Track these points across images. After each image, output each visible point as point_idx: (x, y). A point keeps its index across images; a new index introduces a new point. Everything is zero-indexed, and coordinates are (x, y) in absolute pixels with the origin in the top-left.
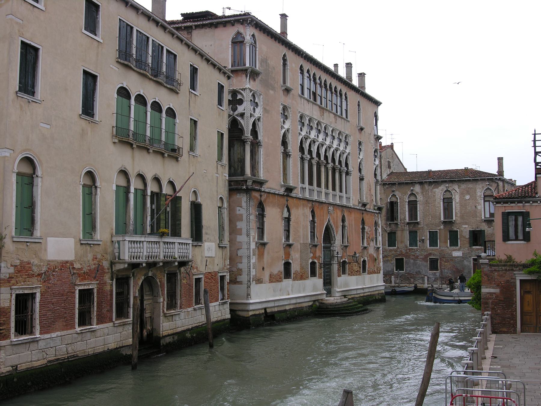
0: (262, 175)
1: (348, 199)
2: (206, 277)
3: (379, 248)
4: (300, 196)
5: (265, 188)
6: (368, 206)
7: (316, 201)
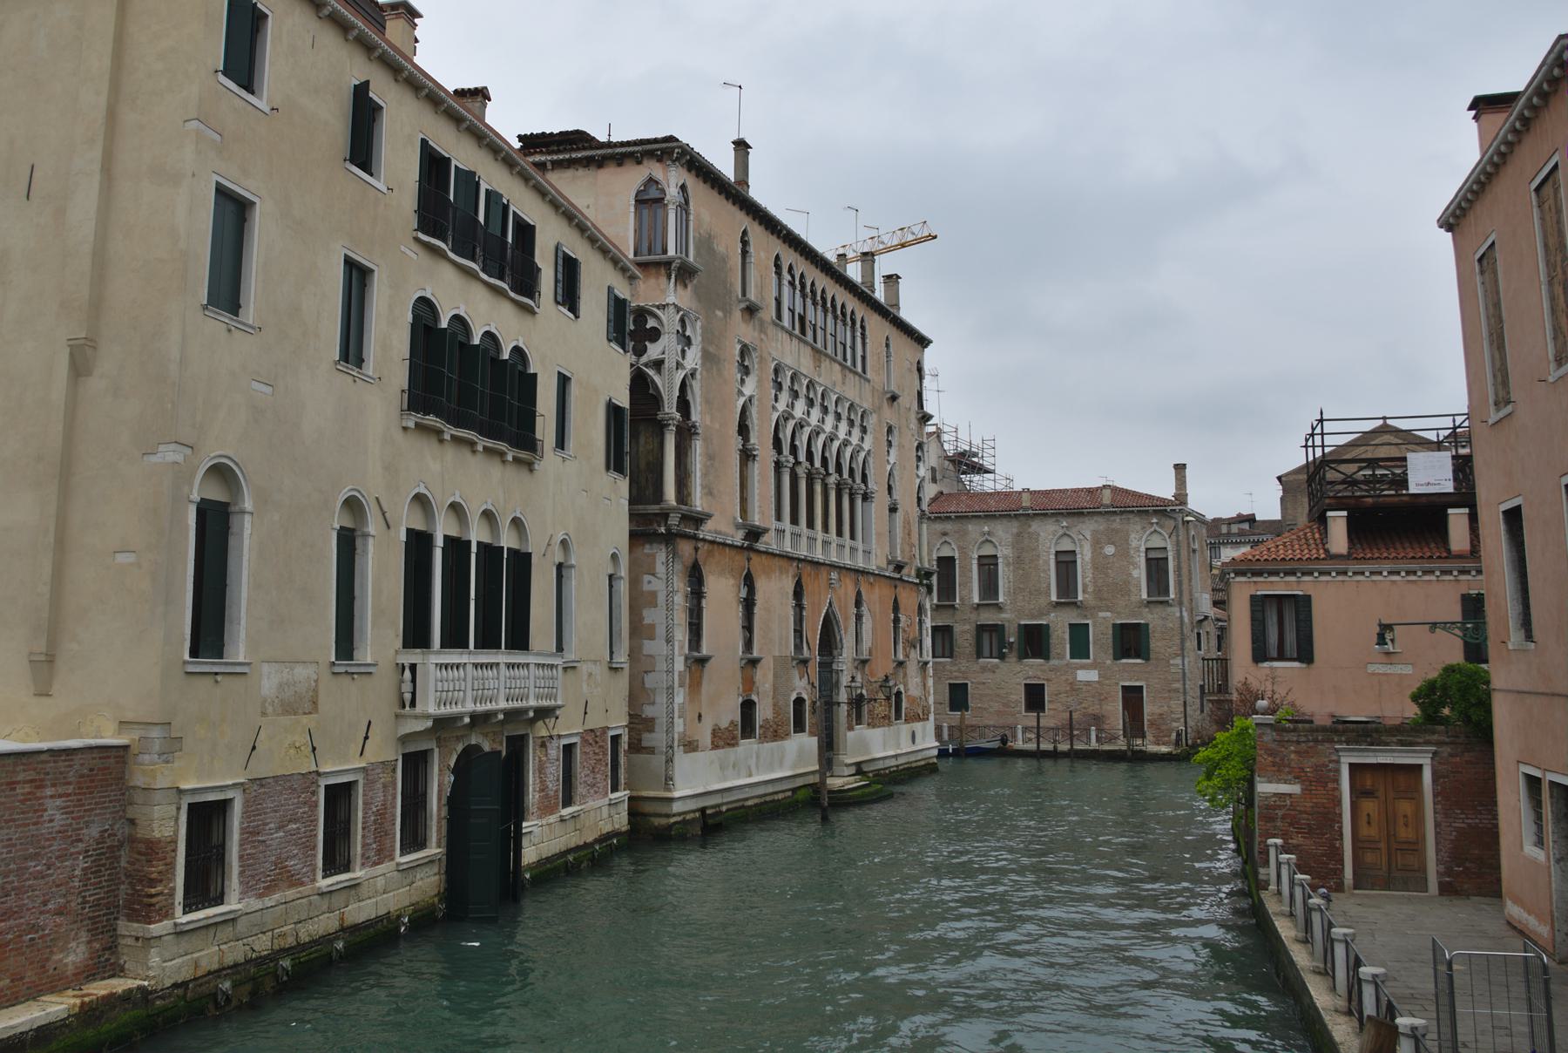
0: (699, 502)
1: (867, 553)
2: (584, 741)
3: (926, 663)
4: (774, 547)
5: (707, 531)
6: (905, 571)
7: (804, 561)
